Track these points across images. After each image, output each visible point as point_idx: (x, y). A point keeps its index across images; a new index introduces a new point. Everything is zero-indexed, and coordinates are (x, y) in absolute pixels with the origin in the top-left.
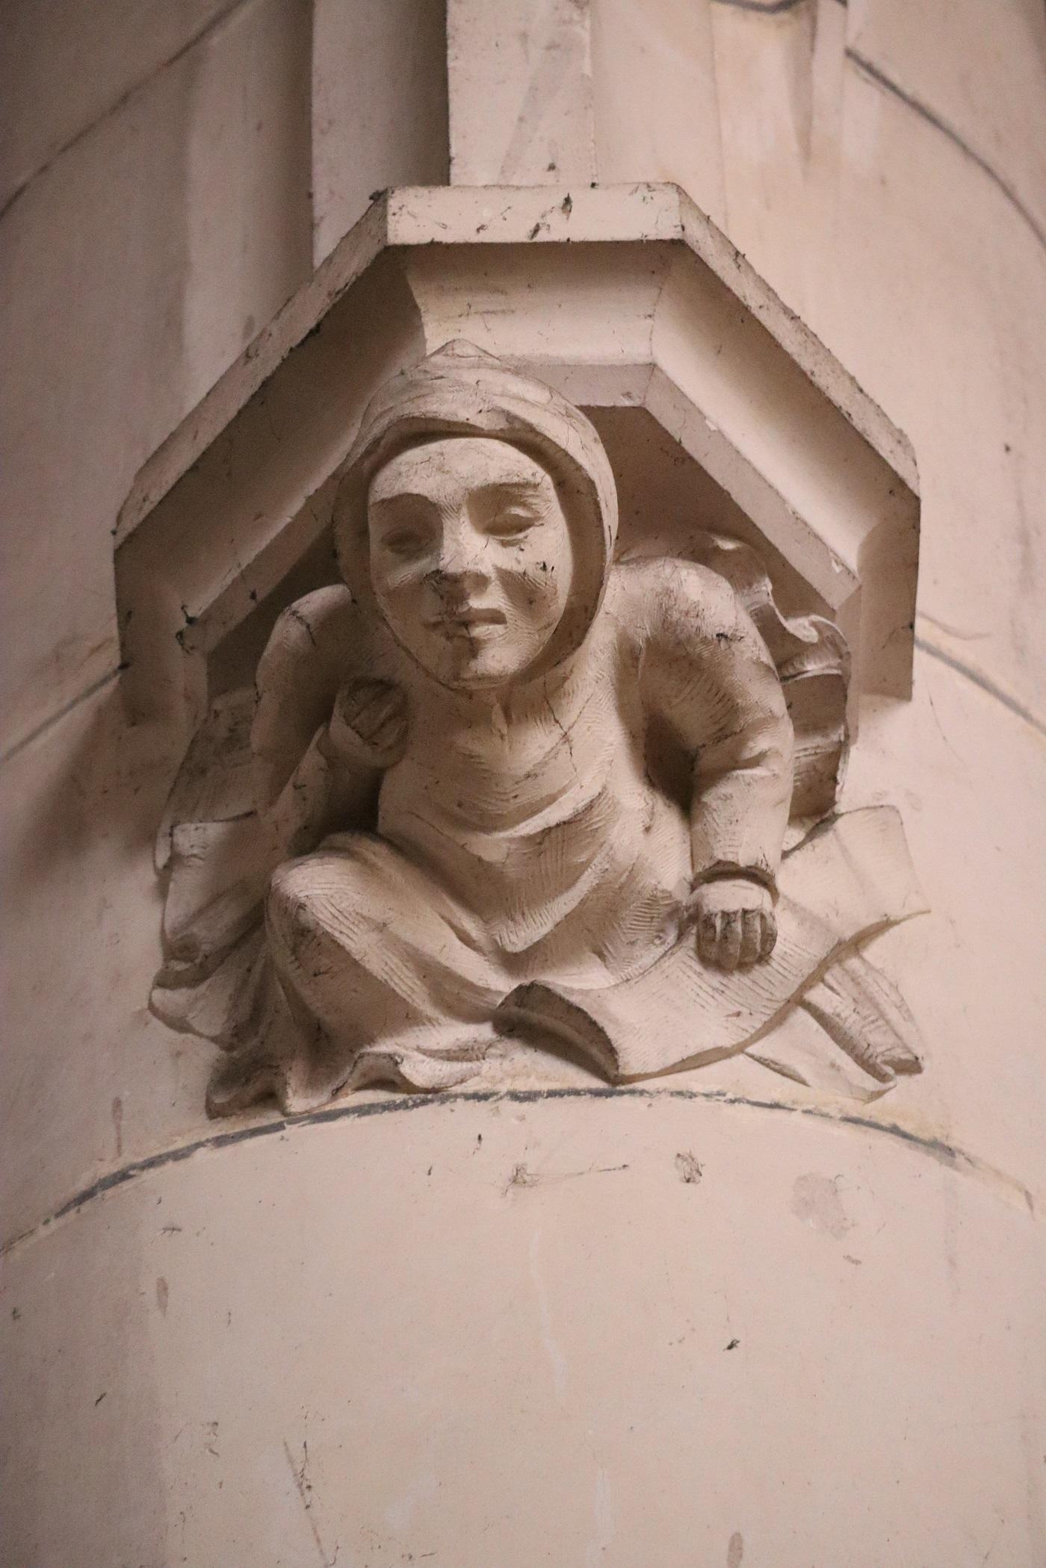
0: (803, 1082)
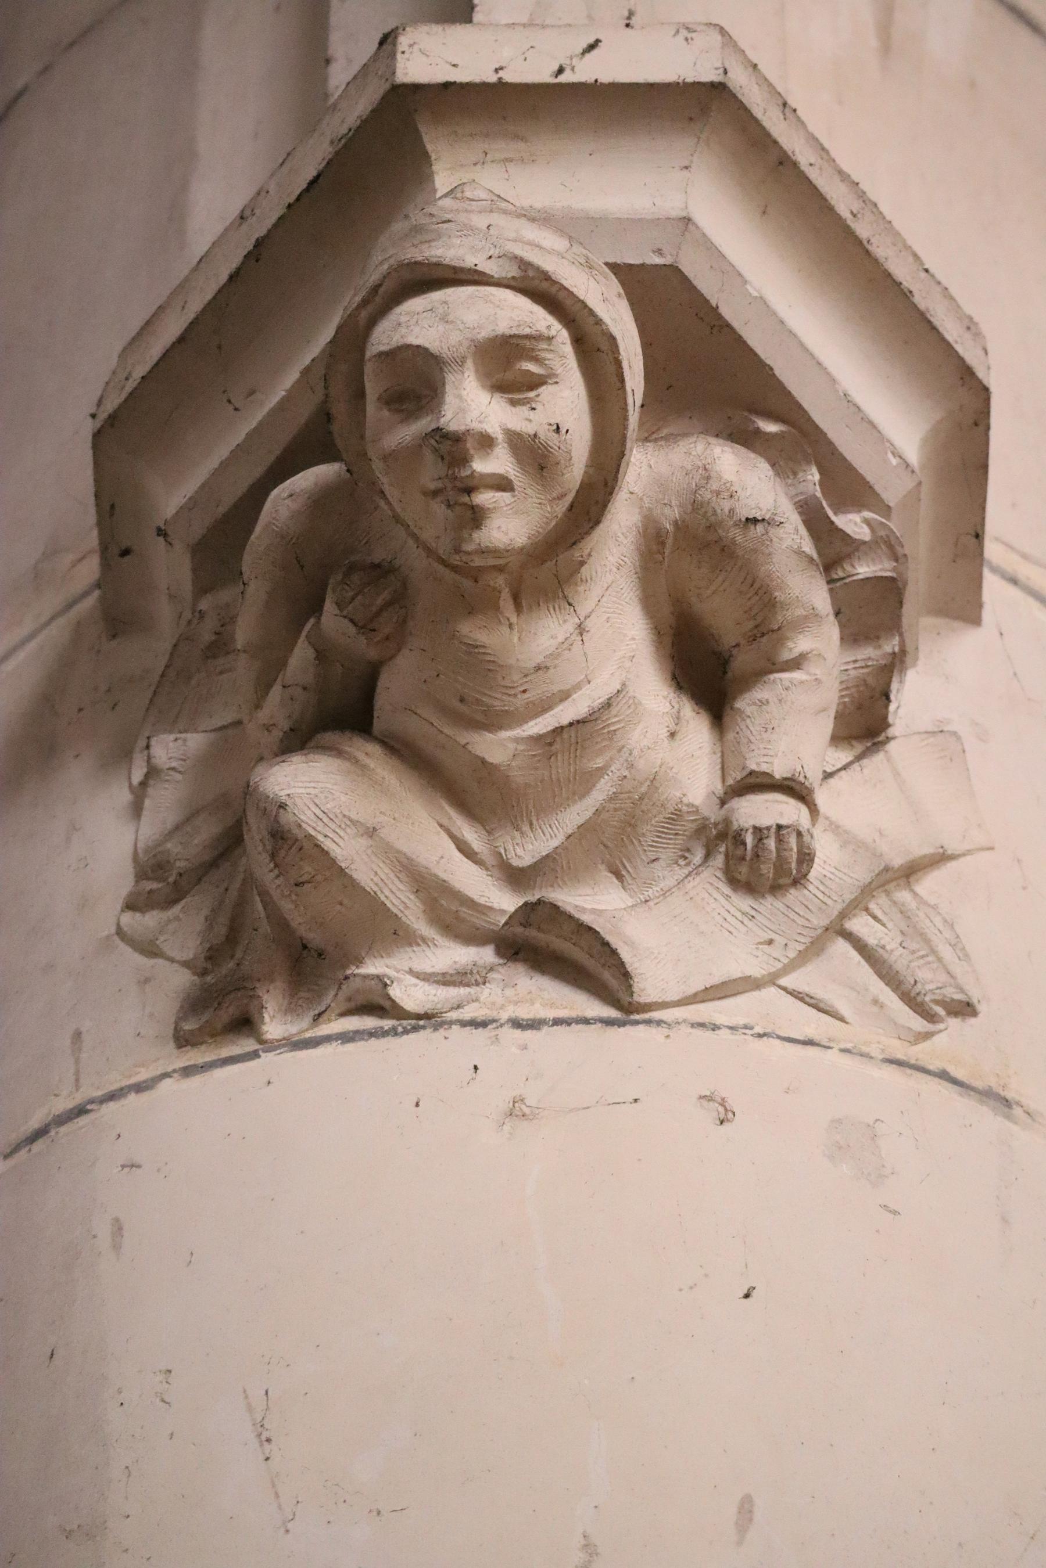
0: (842, 1019)
